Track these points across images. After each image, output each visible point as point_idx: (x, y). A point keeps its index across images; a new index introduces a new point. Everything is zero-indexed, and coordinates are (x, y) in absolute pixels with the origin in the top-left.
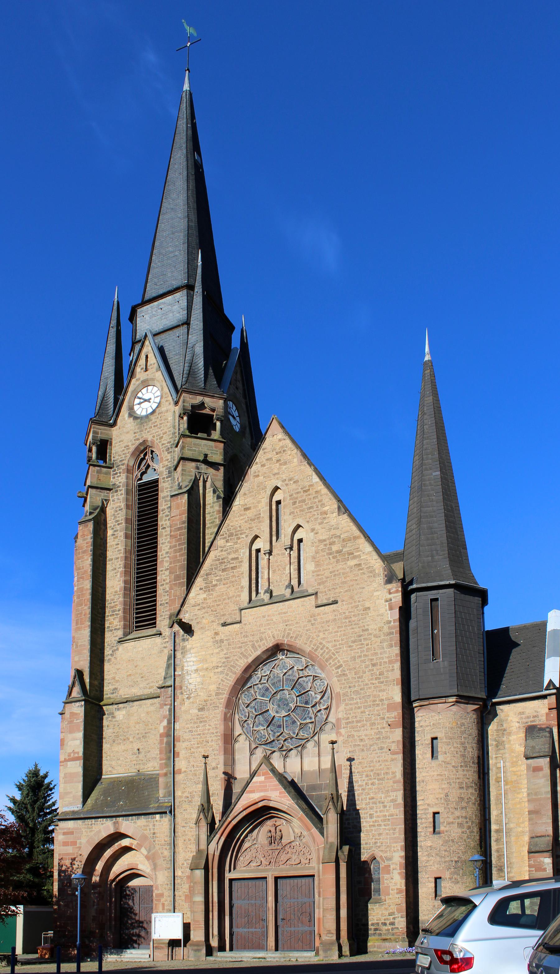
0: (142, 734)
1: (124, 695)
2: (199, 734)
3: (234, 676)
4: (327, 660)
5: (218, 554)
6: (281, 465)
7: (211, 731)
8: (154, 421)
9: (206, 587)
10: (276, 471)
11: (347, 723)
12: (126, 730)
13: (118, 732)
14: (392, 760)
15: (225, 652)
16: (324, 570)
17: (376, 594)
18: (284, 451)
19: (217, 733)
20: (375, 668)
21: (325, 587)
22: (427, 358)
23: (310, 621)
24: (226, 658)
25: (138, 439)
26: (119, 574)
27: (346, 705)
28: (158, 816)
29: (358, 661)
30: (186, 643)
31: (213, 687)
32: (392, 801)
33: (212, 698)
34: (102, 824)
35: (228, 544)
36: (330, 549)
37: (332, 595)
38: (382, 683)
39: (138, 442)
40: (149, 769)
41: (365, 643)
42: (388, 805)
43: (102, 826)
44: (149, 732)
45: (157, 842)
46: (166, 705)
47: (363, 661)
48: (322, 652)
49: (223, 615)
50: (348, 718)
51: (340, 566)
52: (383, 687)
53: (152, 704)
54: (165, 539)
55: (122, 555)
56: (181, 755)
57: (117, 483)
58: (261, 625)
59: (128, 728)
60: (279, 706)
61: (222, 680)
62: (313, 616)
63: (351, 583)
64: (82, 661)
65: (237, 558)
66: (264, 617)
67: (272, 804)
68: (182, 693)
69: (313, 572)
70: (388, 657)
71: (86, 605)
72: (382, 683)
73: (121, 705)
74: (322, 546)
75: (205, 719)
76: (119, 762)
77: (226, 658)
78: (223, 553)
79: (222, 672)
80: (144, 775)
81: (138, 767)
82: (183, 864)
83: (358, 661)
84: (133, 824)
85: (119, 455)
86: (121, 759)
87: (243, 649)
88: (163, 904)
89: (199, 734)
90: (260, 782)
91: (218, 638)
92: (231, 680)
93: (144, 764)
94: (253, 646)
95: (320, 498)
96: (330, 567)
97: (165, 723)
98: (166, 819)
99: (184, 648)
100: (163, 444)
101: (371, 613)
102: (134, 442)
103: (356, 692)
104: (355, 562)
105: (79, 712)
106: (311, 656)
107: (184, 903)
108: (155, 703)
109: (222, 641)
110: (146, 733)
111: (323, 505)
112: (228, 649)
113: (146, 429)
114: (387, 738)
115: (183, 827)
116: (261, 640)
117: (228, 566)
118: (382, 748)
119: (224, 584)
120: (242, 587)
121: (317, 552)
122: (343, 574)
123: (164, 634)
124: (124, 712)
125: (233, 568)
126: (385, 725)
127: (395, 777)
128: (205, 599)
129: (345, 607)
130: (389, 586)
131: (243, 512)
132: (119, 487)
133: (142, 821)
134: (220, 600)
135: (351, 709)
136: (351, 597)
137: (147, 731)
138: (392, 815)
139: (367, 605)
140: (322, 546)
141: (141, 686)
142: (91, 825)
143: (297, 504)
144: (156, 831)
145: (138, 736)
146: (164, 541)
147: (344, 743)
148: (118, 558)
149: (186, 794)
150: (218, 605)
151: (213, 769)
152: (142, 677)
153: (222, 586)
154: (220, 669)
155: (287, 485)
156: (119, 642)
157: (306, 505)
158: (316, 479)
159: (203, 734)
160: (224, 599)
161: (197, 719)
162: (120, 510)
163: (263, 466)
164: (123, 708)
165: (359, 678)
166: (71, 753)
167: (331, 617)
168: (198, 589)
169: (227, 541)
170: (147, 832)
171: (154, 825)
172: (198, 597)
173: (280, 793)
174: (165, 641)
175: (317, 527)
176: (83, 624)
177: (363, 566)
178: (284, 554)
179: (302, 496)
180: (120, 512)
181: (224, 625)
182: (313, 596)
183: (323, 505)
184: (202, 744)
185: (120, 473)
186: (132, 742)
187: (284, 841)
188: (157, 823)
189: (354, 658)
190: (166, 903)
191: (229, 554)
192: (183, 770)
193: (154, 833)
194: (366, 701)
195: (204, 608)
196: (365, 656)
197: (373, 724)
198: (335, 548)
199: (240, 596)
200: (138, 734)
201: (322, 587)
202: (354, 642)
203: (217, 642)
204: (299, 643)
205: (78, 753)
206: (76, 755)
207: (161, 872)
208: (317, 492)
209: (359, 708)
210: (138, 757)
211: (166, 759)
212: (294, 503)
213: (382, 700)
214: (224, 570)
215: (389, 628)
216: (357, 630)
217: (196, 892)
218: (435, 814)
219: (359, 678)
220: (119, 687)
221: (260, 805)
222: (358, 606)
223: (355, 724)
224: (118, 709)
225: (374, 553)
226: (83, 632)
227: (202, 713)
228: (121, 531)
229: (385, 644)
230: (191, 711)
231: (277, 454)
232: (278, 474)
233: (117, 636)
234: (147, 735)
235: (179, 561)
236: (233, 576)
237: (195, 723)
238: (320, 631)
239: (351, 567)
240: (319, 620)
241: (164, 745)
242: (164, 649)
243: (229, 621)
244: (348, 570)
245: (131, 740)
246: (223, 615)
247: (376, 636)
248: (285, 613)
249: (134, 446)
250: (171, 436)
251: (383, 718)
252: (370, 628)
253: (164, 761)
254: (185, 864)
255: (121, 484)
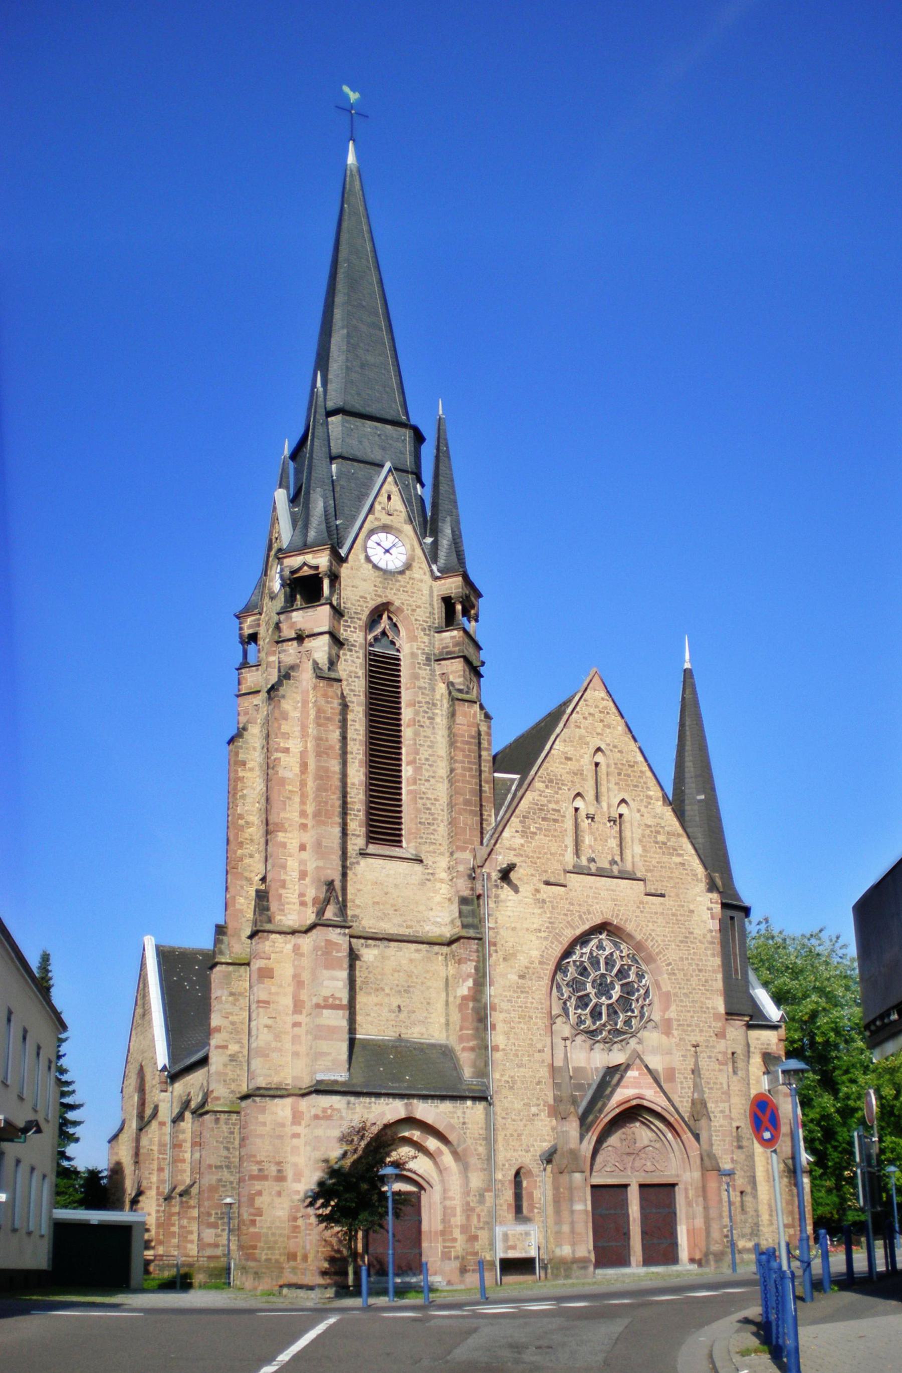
0: (403, 986)
1: (370, 928)
2: (521, 1007)
3: (560, 946)
4: (658, 954)
5: (536, 798)
6: (604, 726)
7: (535, 1005)
8: (402, 583)
9: (523, 831)
10: (599, 730)
11: (679, 1025)
12: (379, 977)
13: (366, 977)
14: (720, 1070)
15: (549, 915)
16: (651, 857)
17: (698, 899)
18: (608, 713)
19: (542, 1008)
20: (701, 974)
21: (652, 876)
22: (687, 665)
23: (638, 907)
24: (550, 923)
25: (380, 596)
26: (357, 761)
27: (677, 1006)
28: (469, 1103)
29: (686, 962)
30: (500, 892)
31: (535, 954)
32: (722, 1112)
33: (534, 965)
34: (387, 1104)
35: (547, 791)
36: (655, 837)
37: (660, 887)
38: (707, 990)
39: (379, 601)
40: (415, 1036)
41: (692, 946)
42: (718, 1115)
43: (387, 1107)
44: (414, 987)
45: (468, 1135)
46: (470, 960)
47: (690, 964)
48: (652, 944)
49: (546, 872)
50: (679, 1020)
51: (665, 859)
52: (708, 996)
53: (417, 951)
54: (424, 741)
55: (361, 737)
56: (497, 1027)
57: (351, 639)
58: (588, 896)
59: (383, 974)
60: (599, 990)
61: (546, 948)
62: (641, 902)
63: (677, 881)
64: (328, 868)
65: (559, 811)
66: (591, 888)
67: (646, 1103)
68: (496, 951)
69: (641, 856)
70: (712, 966)
71: (334, 793)
72: (707, 990)
73: (370, 942)
74: (648, 832)
75: (527, 989)
76: (370, 1019)
77: (550, 923)
78: (542, 798)
79: (546, 938)
80: (407, 1041)
81: (397, 1029)
82: (504, 1165)
83: (686, 962)
84: (433, 1108)
85: (352, 604)
86: (372, 1015)
87: (570, 919)
88: (479, 1216)
89: (521, 1007)
90: (634, 1078)
91: (538, 896)
92: (557, 951)
93: (406, 1027)
94: (580, 917)
95: (644, 780)
96: (657, 856)
97: (470, 983)
98: (480, 1106)
99: (497, 896)
100: (416, 620)
101: (695, 917)
102: (374, 597)
103: (685, 995)
104: (678, 860)
105: (340, 942)
106: (639, 947)
107: (506, 1214)
108: (420, 950)
109: (544, 901)
110: (409, 987)
111: (648, 788)
112: (551, 913)
113: (391, 589)
114: (714, 1047)
115: (504, 1118)
116: (589, 913)
117: (549, 816)
118: (710, 1057)
119: (545, 836)
120: (566, 846)
121: (644, 836)
122: (670, 868)
123: (425, 862)
124: (375, 951)
125: (555, 821)
126: (713, 1035)
127: (722, 1088)
128: (522, 845)
129: (672, 903)
130: (710, 895)
131: (563, 760)
132: (353, 645)
133: (447, 1106)
134: (540, 853)
135: (682, 1011)
136: (677, 895)
137: (409, 984)
138: (721, 1126)
139: (692, 907)
140: (648, 832)
141: (395, 921)
142: (370, 1103)
143: (622, 777)
144: (466, 1120)
145: (397, 989)
146: (422, 742)
147: (676, 1045)
148: (355, 740)
149: (506, 1078)
150: (539, 858)
151: (539, 1051)
152: (396, 910)
153: (542, 837)
154: (543, 934)
155: (611, 751)
156: (361, 854)
157: (632, 781)
158: (640, 758)
159: (526, 1007)
160: (546, 853)
161: (518, 987)
162: (356, 677)
163: (585, 718)
164: (375, 946)
165: (688, 980)
166: (328, 997)
167: (660, 910)
168: (514, 830)
169: (547, 787)
170: (454, 1121)
171: (464, 1113)
172: (513, 840)
173: (655, 1092)
174: (427, 871)
175: (643, 809)
176: (330, 818)
177: (687, 867)
178: (605, 824)
179: (627, 770)
180: (356, 680)
181: (547, 883)
182: (642, 882)
183: (648, 788)
184: (524, 1019)
185: (355, 628)
186: (388, 995)
187: (639, 1145)
188: (468, 1111)
189: (682, 959)
190: (483, 1214)
191: (549, 802)
192: (501, 1047)
193: (464, 1123)
194: (694, 1007)
195: (522, 856)
196: (692, 959)
197: (701, 1031)
198: (661, 838)
199: (563, 855)
200: (397, 986)
201: (649, 874)
202: (681, 942)
203: (538, 900)
204: (630, 927)
205: (340, 999)
206: (337, 1002)
207: (475, 1174)
208: (641, 772)
209: (689, 1011)
210: (397, 1016)
211: (473, 1029)
212: (619, 774)
213: (708, 1008)
214: (544, 819)
215: (712, 937)
216: (683, 930)
217: (577, 1199)
218: (738, 1128)
219: (688, 980)
220: (361, 915)
221: (634, 1103)
222: (683, 906)
223: (685, 1027)
224: (367, 946)
225: (696, 857)
226: (329, 829)
227: (523, 981)
228: (358, 705)
229: (709, 952)
230: (509, 976)
231: (601, 712)
232: (602, 735)
233: (355, 844)
234: (411, 989)
235: (469, 783)
236: (556, 830)
237: (515, 992)
238: (649, 921)
239: (676, 864)
240: (647, 910)
241: (470, 1011)
242: (428, 883)
243: (552, 880)
244: (673, 865)
245: (387, 991)
246: (546, 872)
247: (700, 942)
248: (613, 890)
249: (374, 602)
250: (428, 615)
251: (710, 1027)
252: (695, 931)
253: (470, 1032)
254: (507, 1165)
255: (357, 644)
